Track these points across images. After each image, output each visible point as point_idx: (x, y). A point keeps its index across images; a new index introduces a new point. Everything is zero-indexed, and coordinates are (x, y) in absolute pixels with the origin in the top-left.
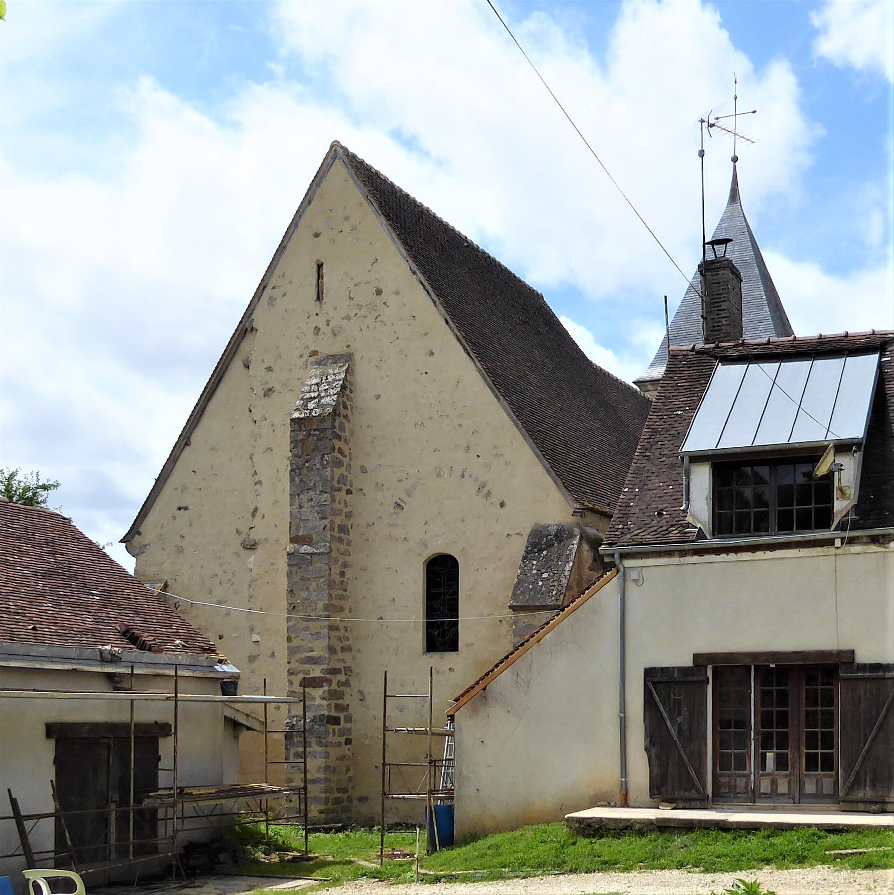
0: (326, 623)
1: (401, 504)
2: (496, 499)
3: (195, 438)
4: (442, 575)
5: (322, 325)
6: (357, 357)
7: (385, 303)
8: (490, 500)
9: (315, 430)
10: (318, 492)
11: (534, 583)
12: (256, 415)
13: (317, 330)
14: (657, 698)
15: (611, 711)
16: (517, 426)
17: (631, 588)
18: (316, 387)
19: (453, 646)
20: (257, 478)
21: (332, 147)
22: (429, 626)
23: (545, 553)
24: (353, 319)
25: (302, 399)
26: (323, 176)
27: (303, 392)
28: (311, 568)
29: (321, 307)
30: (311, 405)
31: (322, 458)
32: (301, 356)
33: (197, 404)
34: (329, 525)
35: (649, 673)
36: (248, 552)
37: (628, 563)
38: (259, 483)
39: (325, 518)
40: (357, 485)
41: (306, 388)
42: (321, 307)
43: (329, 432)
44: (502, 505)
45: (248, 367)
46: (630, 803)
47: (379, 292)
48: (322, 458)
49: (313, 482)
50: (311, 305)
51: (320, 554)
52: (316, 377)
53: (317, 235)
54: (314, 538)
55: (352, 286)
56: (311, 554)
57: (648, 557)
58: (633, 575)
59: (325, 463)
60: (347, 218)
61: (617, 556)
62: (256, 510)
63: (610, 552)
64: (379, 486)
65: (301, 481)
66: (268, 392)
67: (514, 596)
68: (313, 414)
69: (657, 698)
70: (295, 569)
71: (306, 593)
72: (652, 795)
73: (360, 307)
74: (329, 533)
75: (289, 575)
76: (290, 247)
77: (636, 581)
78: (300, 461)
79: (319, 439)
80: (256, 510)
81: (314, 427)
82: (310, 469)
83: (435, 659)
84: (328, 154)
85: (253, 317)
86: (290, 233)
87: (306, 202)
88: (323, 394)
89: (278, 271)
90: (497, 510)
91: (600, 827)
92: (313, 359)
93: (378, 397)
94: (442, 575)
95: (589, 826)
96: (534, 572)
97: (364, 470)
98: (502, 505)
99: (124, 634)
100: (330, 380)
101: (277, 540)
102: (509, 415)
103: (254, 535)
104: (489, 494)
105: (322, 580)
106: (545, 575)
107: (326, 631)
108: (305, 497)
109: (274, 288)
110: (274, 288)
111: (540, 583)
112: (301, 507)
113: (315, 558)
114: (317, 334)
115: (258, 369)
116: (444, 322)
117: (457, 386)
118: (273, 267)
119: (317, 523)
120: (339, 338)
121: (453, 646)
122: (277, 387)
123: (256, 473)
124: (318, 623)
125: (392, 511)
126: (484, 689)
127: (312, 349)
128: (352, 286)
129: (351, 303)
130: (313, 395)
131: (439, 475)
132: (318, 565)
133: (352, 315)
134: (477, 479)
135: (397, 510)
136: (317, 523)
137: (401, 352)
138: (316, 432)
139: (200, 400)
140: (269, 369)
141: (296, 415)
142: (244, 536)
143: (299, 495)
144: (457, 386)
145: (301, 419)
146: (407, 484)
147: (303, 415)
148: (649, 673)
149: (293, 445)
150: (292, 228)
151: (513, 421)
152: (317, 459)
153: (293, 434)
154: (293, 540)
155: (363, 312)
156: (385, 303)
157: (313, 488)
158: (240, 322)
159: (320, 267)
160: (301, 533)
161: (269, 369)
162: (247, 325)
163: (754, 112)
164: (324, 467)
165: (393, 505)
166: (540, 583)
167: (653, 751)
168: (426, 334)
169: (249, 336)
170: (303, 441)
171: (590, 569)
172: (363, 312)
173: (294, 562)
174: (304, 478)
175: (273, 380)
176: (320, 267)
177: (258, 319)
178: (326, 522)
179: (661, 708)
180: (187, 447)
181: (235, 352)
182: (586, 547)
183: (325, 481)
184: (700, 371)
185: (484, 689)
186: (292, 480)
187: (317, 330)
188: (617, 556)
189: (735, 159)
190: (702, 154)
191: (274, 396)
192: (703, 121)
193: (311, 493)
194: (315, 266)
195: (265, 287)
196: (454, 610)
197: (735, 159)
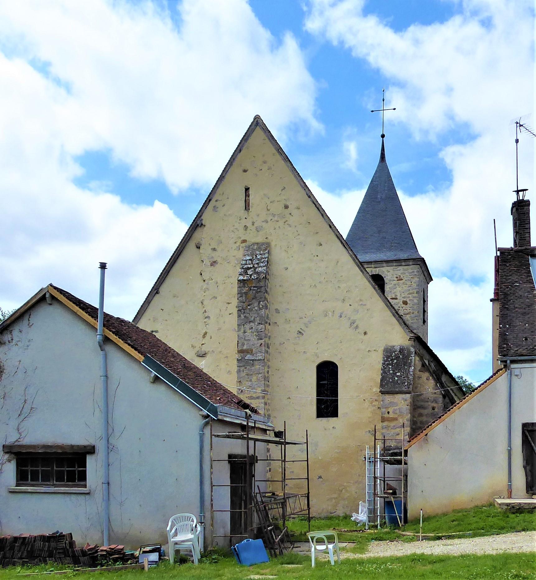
0: (263, 401)
1: (302, 331)
2: (361, 330)
3: (162, 289)
4: (327, 374)
5: (249, 225)
6: (273, 244)
7: (290, 214)
8: (357, 331)
9: (254, 287)
10: (256, 324)
11: (393, 378)
12: (206, 276)
13: (246, 227)
14: (530, 439)
15: (502, 447)
16: (375, 288)
17: (514, 379)
18: (250, 262)
19: (334, 413)
20: (206, 315)
21: (255, 119)
22: (319, 402)
23: (395, 361)
24: (270, 223)
25: (242, 268)
26: (249, 136)
27: (242, 264)
28: (253, 368)
29: (248, 214)
30: (250, 272)
31: (259, 304)
32: (235, 243)
33: (165, 269)
34: (263, 343)
35: (525, 425)
36: (201, 358)
37: (513, 366)
38: (208, 317)
39: (261, 339)
40: (273, 320)
41: (244, 262)
42: (248, 214)
43: (263, 289)
44: (365, 333)
45: (199, 248)
46: (512, 497)
47: (286, 207)
48: (259, 304)
49: (253, 317)
50: (243, 213)
51: (259, 360)
52: (248, 255)
53: (245, 171)
54: (254, 350)
55: (268, 203)
56: (253, 360)
57: (517, 363)
58: (517, 372)
59: (261, 306)
60: (265, 162)
61: (508, 362)
62: (206, 333)
63: (505, 360)
64: (287, 321)
65: (245, 317)
66: (214, 263)
67: (382, 385)
68: (253, 277)
69: (530, 439)
70: (242, 369)
71: (250, 383)
72: (527, 492)
73: (274, 215)
74: (263, 348)
75: (239, 372)
76: (228, 177)
77: (517, 375)
78: (245, 305)
79: (257, 292)
80: (206, 333)
81: (253, 285)
82: (251, 310)
83: (324, 421)
84: (252, 123)
85: (202, 218)
86: (227, 169)
87: (238, 151)
88: (256, 266)
89: (220, 191)
90: (362, 336)
91: (519, 508)
92: (244, 245)
93: (287, 269)
94: (327, 374)
95: (513, 507)
96: (391, 372)
97: (277, 311)
98: (365, 333)
99: (238, 403)
100: (259, 257)
101: (220, 352)
102: (369, 282)
103: (204, 349)
104: (357, 327)
105: (260, 375)
106: (398, 374)
107: (263, 405)
108: (247, 326)
109: (216, 201)
110: (216, 201)
111: (396, 378)
112: (245, 332)
113: (256, 362)
114: (246, 230)
115: (206, 250)
116: (328, 226)
117: (337, 264)
118: (216, 188)
119: (256, 342)
120: (260, 233)
121: (334, 413)
122: (219, 260)
123: (205, 311)
124: (257, 401)
125: (296, 335)
126: (426, 435)
127: (242, 239)
128: (268, 203)
129: (269, 212)
130: (249, 266)
131: (326, 316)
132: (258, 367)
133: (269, 220)
134: (349, 318)
135: (300, 335)
136: (256, 342)
137: (301, 243)
138: (256, 289)
139: (166, 266)
140: (214, 249)
141: (241, 278)
142: (197, 349)
143: (244, 325)
144: (337, 264)
145: (245, 280)
146: (306, 320)
147: (245, 278)
148: (525, 425)
149: (239, 295)
150: (229, 166)
151: (372, 285)
152: (256, 304)
153: (239, 289)
154: (240, 352)
155: (276, 218)
156: (290, 214)
157: (253, 322)
158: (194, 221)
159: (247, 189)
160: (245, 347)
161: (214, 249)
162: (198, 222)
163: (394, 109)
164: (260, 309)
165: (296, 332)
166: (396, 378)
167: (528, 468)
168: (317, 233)
169: (199, 230)
170: (246, 293)
171: (420, 371)
172: (276, 218)
173: (241, 365)
174: (247, 315)
175: (216, 256)
176: (247, 189)
177: (206, 219)
178: (262, 341)
179: (533, 444)
180: (157, 295)
181: (191, 237)
182: (417, 358)
183: (261, 317)
184: (520, 262)
185: (426, 435)
186: (239, 316)
187: (246, 227)
188: (508, 362)
189: (383, 136)
190: (517, 141)
191: (217, 266)
192: (517, 123)
193: (252, 324)
194: (244, 189)
195: (210, 200)
196: (335, 393)
197: (383, 136)
